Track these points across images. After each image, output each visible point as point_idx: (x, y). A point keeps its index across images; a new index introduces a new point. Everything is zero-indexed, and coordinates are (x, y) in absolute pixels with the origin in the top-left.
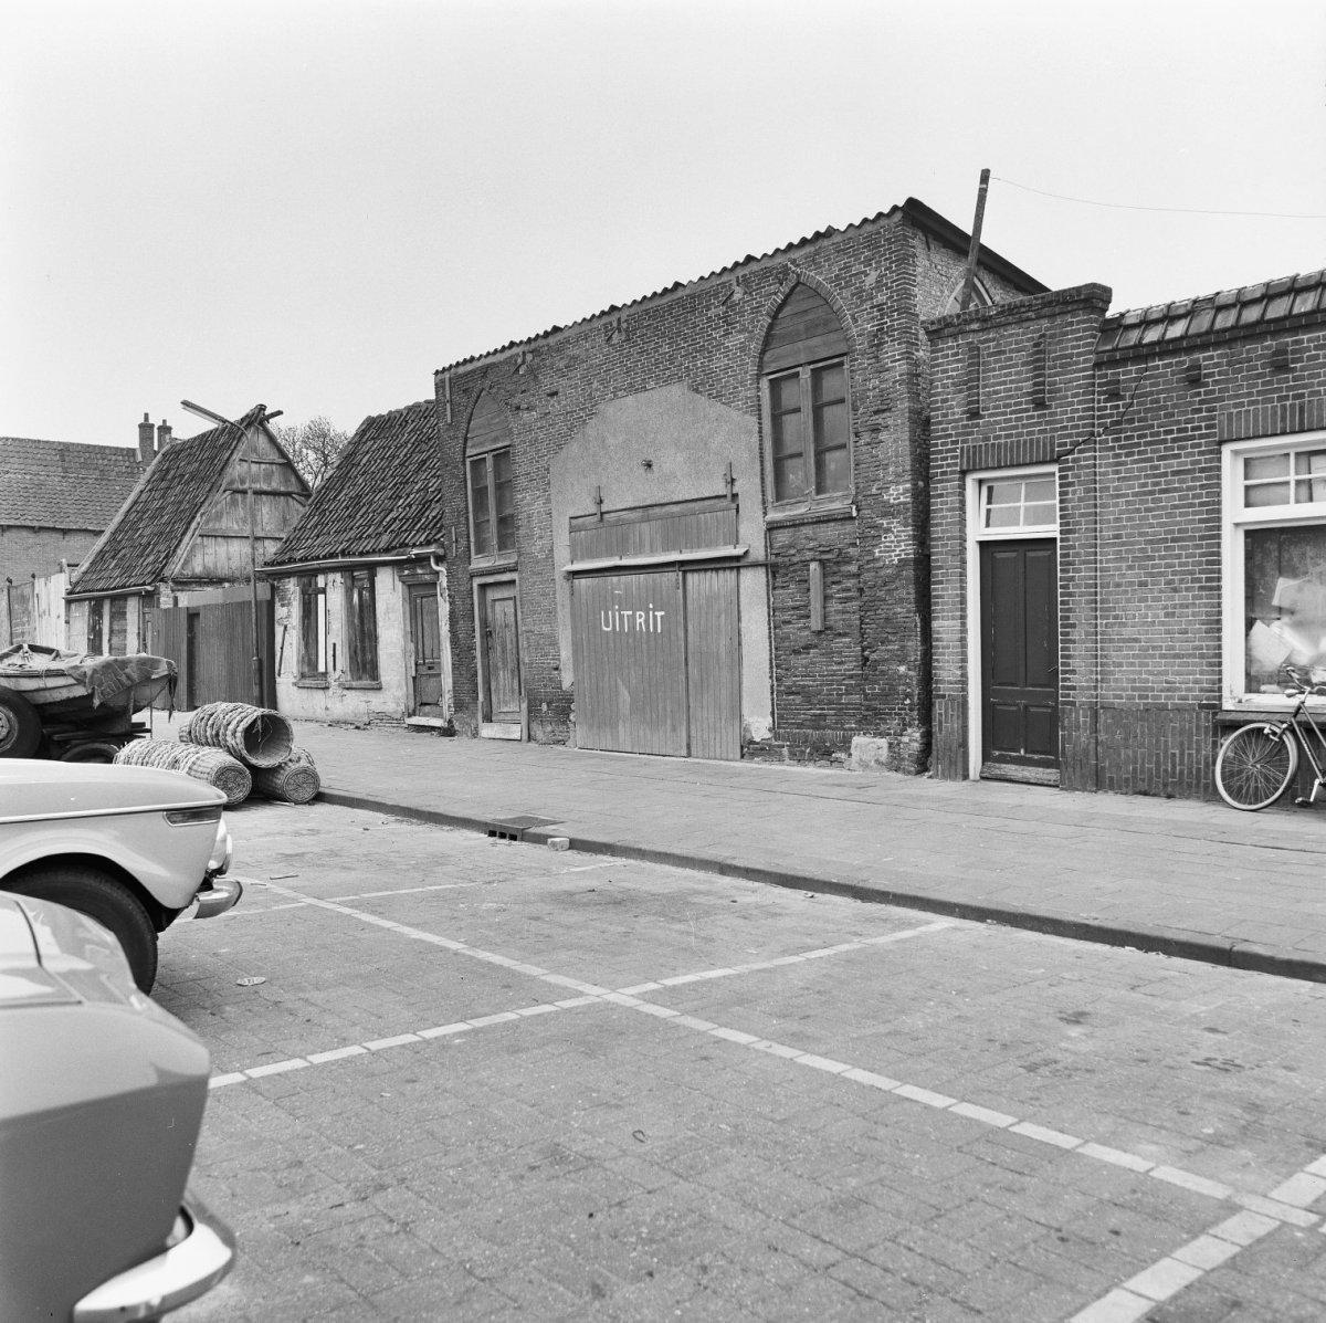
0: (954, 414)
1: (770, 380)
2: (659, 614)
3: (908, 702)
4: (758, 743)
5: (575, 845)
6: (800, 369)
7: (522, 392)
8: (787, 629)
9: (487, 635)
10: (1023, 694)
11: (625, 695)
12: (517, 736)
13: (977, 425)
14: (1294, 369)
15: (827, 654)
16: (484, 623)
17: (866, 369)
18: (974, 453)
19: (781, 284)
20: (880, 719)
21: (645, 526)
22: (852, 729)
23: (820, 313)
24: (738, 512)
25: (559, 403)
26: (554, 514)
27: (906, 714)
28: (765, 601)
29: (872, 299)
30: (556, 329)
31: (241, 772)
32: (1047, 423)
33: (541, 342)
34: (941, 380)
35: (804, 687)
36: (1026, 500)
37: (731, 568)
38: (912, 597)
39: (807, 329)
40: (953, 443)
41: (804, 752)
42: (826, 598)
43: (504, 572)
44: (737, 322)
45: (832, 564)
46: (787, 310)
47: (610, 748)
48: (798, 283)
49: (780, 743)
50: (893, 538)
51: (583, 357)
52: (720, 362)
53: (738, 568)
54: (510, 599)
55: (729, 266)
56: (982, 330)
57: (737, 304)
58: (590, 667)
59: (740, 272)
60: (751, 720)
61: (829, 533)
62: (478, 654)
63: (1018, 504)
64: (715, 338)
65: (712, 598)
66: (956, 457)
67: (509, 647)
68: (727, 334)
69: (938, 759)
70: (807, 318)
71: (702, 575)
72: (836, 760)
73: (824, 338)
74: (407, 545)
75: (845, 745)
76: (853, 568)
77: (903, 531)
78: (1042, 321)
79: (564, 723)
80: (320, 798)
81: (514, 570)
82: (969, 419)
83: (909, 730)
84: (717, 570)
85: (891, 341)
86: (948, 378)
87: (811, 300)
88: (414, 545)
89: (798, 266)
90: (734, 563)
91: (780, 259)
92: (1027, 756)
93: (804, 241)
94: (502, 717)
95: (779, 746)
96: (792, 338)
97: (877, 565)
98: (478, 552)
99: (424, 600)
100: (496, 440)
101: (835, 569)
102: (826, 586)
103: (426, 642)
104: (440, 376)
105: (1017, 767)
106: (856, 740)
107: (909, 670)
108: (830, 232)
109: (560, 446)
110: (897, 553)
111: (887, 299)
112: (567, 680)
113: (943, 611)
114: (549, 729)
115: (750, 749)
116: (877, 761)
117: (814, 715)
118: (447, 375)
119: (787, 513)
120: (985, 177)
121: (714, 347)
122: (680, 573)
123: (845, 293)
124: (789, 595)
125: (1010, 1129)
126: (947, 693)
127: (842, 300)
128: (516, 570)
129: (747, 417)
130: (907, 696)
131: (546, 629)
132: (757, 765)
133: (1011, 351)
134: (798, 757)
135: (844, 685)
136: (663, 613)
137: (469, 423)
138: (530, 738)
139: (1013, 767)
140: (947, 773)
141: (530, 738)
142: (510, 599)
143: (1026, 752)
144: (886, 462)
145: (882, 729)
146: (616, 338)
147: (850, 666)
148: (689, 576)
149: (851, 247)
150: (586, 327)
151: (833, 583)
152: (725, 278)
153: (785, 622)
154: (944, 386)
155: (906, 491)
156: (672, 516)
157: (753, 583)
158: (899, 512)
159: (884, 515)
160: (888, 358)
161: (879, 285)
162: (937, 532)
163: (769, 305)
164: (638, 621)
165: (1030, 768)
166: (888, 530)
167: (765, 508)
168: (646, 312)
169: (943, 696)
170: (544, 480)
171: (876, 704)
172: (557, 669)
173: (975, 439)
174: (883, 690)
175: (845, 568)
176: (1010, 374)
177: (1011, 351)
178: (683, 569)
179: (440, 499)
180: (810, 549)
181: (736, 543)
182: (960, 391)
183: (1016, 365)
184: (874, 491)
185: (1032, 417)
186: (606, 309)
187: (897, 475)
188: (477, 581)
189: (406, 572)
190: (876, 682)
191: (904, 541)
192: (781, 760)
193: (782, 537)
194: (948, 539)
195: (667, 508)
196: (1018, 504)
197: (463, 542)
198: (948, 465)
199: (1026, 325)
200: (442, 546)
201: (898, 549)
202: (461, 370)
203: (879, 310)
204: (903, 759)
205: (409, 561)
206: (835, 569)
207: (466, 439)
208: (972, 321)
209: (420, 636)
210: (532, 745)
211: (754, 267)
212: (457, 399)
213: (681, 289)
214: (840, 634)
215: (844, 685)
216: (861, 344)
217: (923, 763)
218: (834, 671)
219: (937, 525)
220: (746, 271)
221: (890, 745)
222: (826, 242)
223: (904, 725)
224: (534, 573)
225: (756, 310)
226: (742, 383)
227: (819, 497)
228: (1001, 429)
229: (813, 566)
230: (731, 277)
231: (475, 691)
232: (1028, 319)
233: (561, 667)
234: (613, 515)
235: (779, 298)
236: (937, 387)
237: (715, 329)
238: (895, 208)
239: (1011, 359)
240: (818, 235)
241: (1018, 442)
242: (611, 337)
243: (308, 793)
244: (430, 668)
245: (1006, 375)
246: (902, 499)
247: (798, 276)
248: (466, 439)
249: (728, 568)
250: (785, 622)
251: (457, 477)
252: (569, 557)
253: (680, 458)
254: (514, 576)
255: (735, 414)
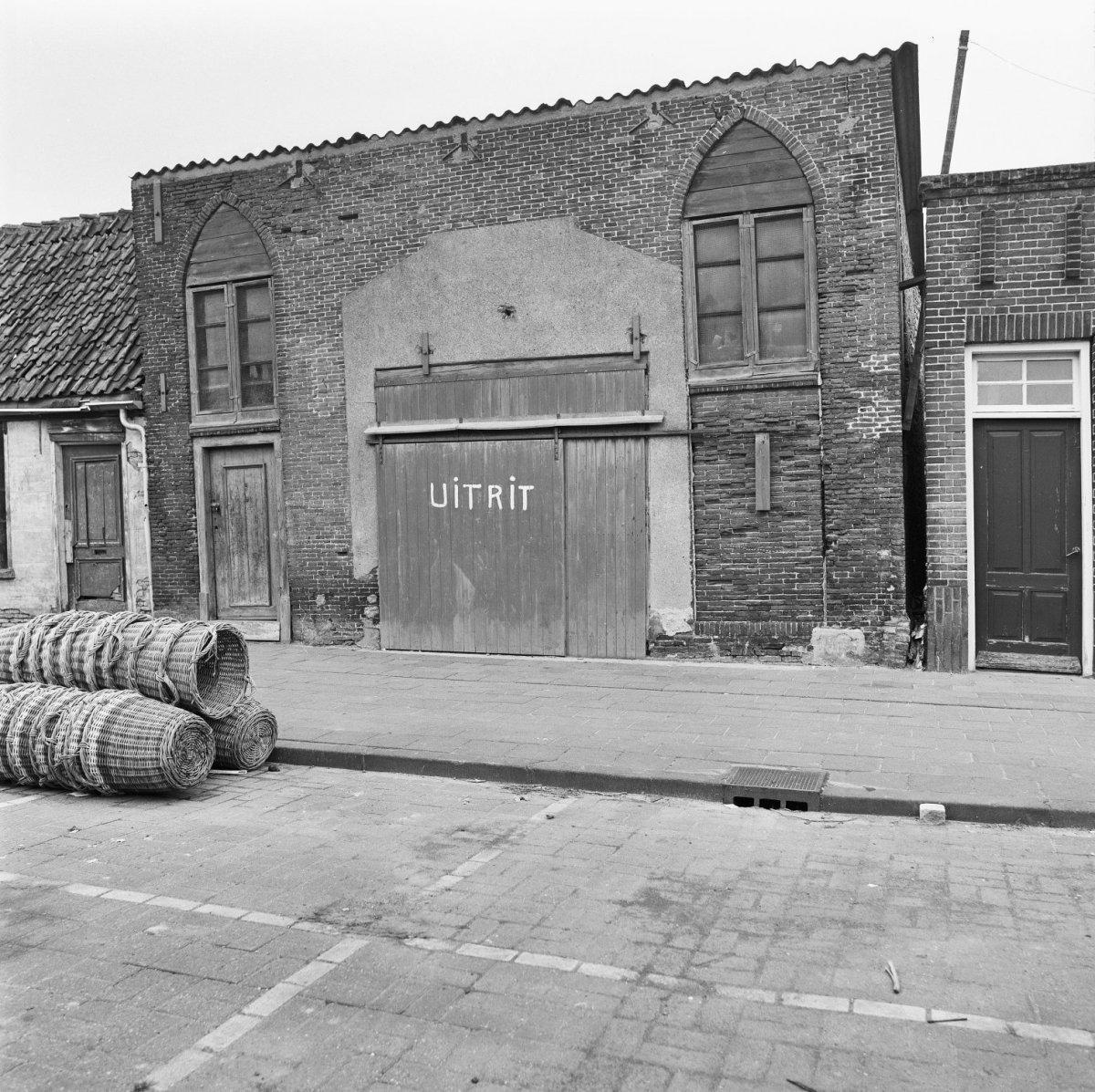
0: (959, 281)
2: (525, 489)
3: (892, 588)
4: (671, 638)
5: (955, 812)
6: (739, 217)
7: (294, 211)
8: (712, 508)
9: (213, 511)
10: (1028, 580)
11: (465, 583)
12: (274, 635)
13: (990, 295)
14: (999, 286)
15: (772, 536)
16: (210, 496)
17: (839, 223)
18: (986, 325)
19: (719, 118)
20: (853, 608)
21: (500, 383)
22: (807, 620)
23: (773, 155)
24: (647, 371)
25: (360, 228)
26: (348, 363)
27: (891, 603)
28: (687, 476)
29: (847, 147)
30: (358, 137)
31: (202, 732)
32: (1080, 298)
33: (328, 152)
34: (941, 243)
35: (737, 573)
36: (1028, 379)
37: (637, 438)
38: (900, 475)
39: (753, 173)
40: (957, 312)
41: (743, 647)
42: (774, 473)
43: (254, 433)
44: (652, 155)
45: (784, 438)
46: (723, 150)
47: (439, 648)
48: (743, 119)
49: (704, 637)
50: (873, 411)
51: (403, 173)
52: (623, 198)
53: (647, 438)
54: (259, 466)
55: (430, 125)
56: (997, 195)
57: (653, 135)
58: (407, 550)
59: (658, 98)
60: (661, 612)
61: (780, 402)
62: (201, 534)
63: (1018, 382)
64: (619, 171)
65: (605, 472)
66: (962, 327)
67: (250, 525)
68: (636, 168)
69: (936, 650)
70: (754, 160)
71: (590, 444)
72: (790, 654)
73: (778, 185)
74: (74, 394)
75: (803, 637)
76: (813, 442)
77: (887, 404)
78: (1074, 192)
79: (355, 618)
80: (279, 757)
81: (274, 430)
82: (977, 287)
83: (894, 620)
84: (614, 439)
85: (874, 196)
86: (950, 242)
87: (759, 141)
88: (88, 394)
89: (743, 100)
90: (642, 432)
91: (718, 90)
92: (1033, 643)
93: (757, 73)
95: (701, 641)
96: (722, 181)
97: (851, 439)
99: (89, 466)
100: (242, 268)
101: (786, 442)
102: (773, 461)
103: (92, 520)
104: (141, 182)
105: (1020, 655)
106: (817, 631)
107: (894, 553)
108: (793, 68)
109: (361, 283)
110: (880, 427)
111: (868, 149)
112: (363, 566)
113: (943, 490)
114: (328, 625)
115: (659, 644)
116: (850, 654)
117: (753, 605)
118: (156, 181)
119: (719, 378)
120: (964, 38)
121: (617, 180)
122: (561, 441)
123: (810, 138)
124: (720, 470)
125: (246, 912)
126: (948, 579)
127: (805, 145)
128: (279, 431)
129: (665, 265)
130: (891, 582)
131: (327, 504)
132: (669, 663)
133: (1034, 220)
134: (732, 650)
135: (797, 571)
136: (532, 487)
137: (194, 244)
138: (293, 638)
139: (1017, 655)
140: (947, 664)
141: (293, 638)
142: (259, 466)
143: (1031, 640)
144: (865, 327)
145: (854, 619)
146: (458, 156)
147: (808, 551)
148: (571, 445)
149: (819, 88)
150: (410, 140)
151: (783, 458)
152: (635, 103)
153: (710, 501)
154: (945, 250)
155: (892, 360)
156: (546, 373)
157: (668, 458)
158: (882, 383)
159: (861, 385)
160: (869, 214)
161: (857, 132)
162: (936, 406)
163: (700, 140)
164: (491, 496)
165: (1038, 656)
166: (864, 402)
167: (687, 371)
168: (510, 130)
169: (944, 583)
170: (333, 320)
171: (849, 592)
172: (344, 553)
173: (987, 309)
174: (857, 576)
175: (801, 442)
176: (1034, 244)
177: (1034, 220)
178: (564, 435)
179: (137, 338)
180: (751, 420)
181: (645, 408)
182: (968, 258)
183: (1041, 235)
184: (847, 358)
185: (1062, 291)
186: (447, 121)
187: (880, 342)
188: (198, 446)
189: (66, 429)
190: (846, 568)
191: (888, 414)
192: (707, 655)
193: (710, 405)
194: (950, 414)
195: (534, 364)
196: (1018, 382)
197: (179, 395)
198: (950, 336)
199: (1056, 193)
200: (140, 396)
201: (880, 423)
202: (183, 176)
203: (857, 161)
204: (888, 651)
205: (83, 414)
206: (786, 442)
207: (188, 264)
208: (988, 183)
209: (82, 510)
210: (298, 645)
211: (678, 94)
213: (564, 108)
214: (790, 515)
215: (797, 571)
216: (831, 196)
217: (916, 654)
218: (784, 555)
219: (934, 399)
220: (668, 97)
221: (867, 635)
222: (783, 78)
223: (886, 614)
224: (309, 436)
225: (684, 143)
226: (659, 226)
227: (764, 361)
228: (1021, 301)
229: (759, 438)
230: (647, 104)
231: (195, 581)
232: (1062, 189)
233: (354, 550)
234: (446, 368)
235: (717, 133)
236: (936, 251)
237: (618, 160)
238: (885, 52)
239: (1034, 228)
240: (778, 68)
241: (1043, 316)
242: (450, 156)
243: (262, 753)
244: (97, 552)
245: (1027, 245)
246: (887, 369)
247: (743, 111)
249: (593, 438)
250: (710, 501)
251: (171, 312)
252: (373, 417)
253: (560, 306)
254: (274, 438)
255: (646, 260)
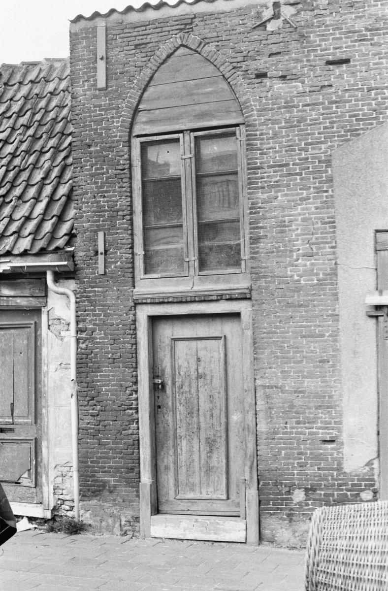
1: (141, 143)
9: (157, 389)
12: (239, 536)
26: (341, 224)
81: (244, 298)
94: (183, 506)
98: (148, 268)
100: (203, 116)
137: (145, 90)
197: (123, 254)
207: (136, 111)
212: (118, 55)
248: (136, 111)
251: (114, 164)
